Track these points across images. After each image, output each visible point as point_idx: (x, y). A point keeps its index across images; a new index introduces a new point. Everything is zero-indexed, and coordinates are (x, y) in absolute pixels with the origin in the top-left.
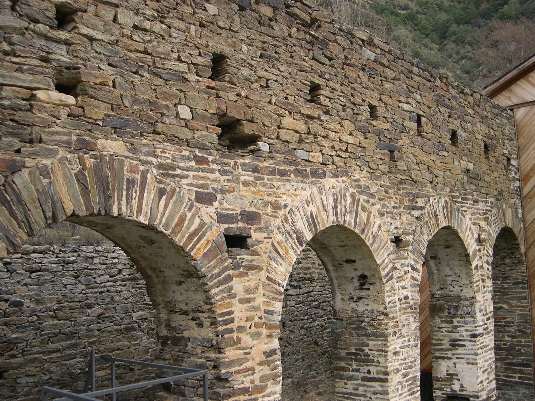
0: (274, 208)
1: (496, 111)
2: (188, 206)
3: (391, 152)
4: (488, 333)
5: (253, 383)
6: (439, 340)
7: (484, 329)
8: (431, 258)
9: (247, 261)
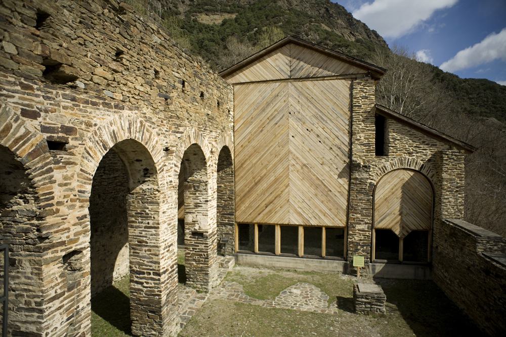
0: (87, 125)
1: (225, 85)
2: (14, 118)
3: (166, 99)
4: (214, 199)
5: (69, 238)
6: (188, 203)
7: (212, 198)
8: (186, 160)
9: (65, 158)
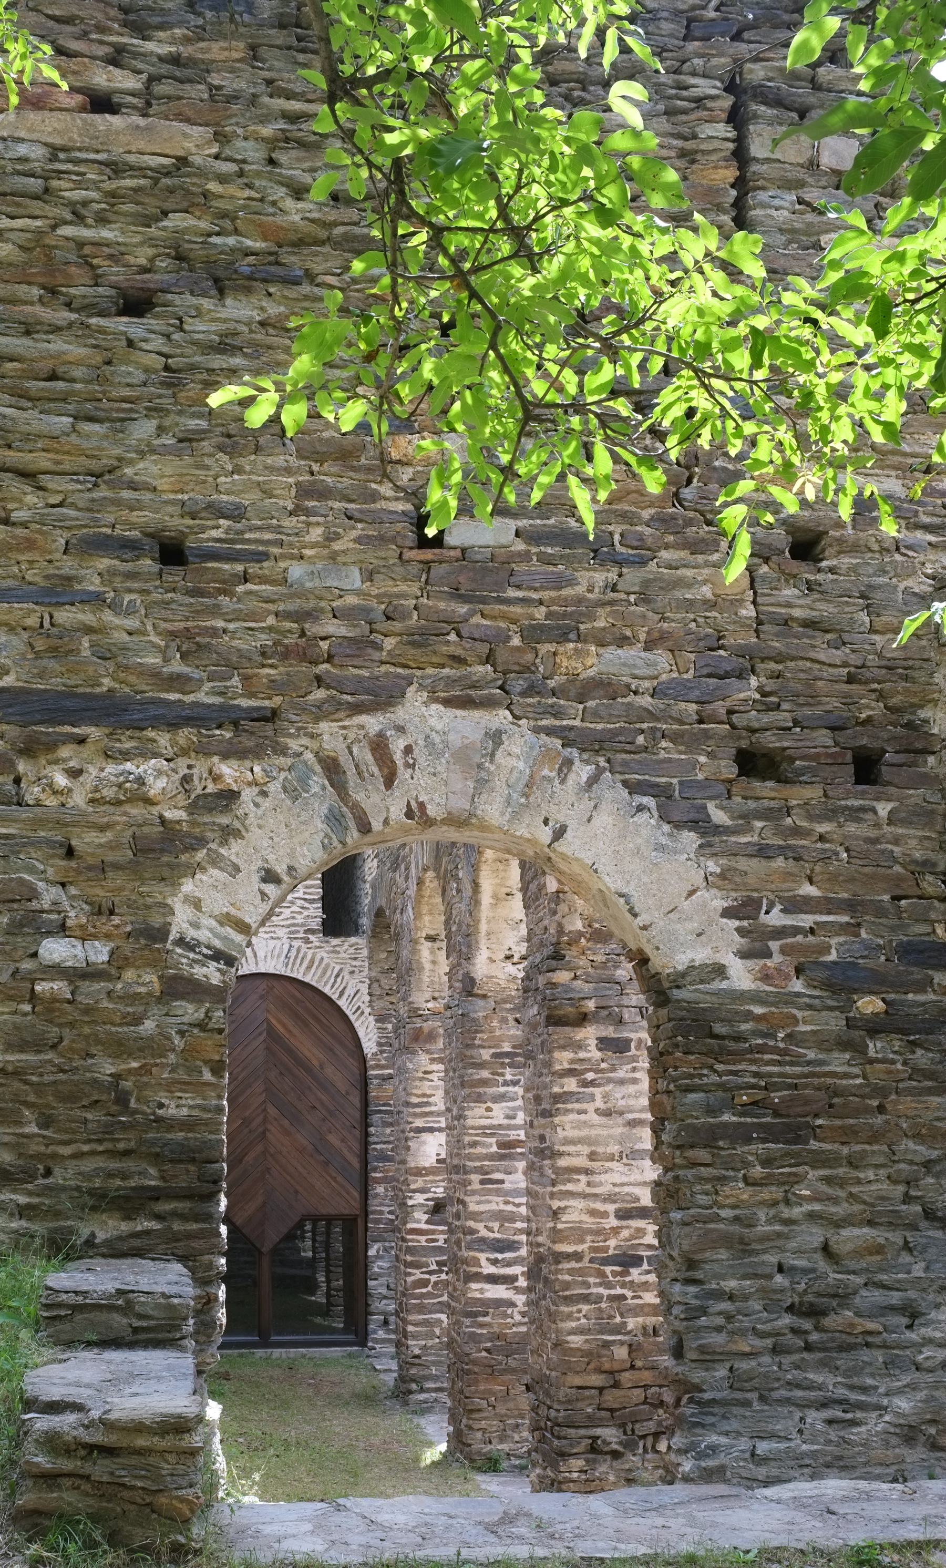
6: (424, 1095)
